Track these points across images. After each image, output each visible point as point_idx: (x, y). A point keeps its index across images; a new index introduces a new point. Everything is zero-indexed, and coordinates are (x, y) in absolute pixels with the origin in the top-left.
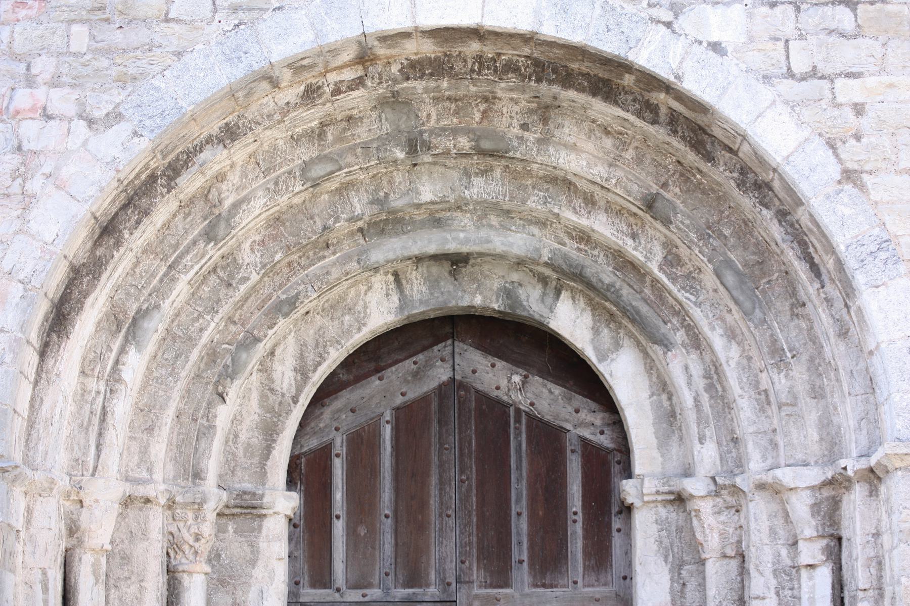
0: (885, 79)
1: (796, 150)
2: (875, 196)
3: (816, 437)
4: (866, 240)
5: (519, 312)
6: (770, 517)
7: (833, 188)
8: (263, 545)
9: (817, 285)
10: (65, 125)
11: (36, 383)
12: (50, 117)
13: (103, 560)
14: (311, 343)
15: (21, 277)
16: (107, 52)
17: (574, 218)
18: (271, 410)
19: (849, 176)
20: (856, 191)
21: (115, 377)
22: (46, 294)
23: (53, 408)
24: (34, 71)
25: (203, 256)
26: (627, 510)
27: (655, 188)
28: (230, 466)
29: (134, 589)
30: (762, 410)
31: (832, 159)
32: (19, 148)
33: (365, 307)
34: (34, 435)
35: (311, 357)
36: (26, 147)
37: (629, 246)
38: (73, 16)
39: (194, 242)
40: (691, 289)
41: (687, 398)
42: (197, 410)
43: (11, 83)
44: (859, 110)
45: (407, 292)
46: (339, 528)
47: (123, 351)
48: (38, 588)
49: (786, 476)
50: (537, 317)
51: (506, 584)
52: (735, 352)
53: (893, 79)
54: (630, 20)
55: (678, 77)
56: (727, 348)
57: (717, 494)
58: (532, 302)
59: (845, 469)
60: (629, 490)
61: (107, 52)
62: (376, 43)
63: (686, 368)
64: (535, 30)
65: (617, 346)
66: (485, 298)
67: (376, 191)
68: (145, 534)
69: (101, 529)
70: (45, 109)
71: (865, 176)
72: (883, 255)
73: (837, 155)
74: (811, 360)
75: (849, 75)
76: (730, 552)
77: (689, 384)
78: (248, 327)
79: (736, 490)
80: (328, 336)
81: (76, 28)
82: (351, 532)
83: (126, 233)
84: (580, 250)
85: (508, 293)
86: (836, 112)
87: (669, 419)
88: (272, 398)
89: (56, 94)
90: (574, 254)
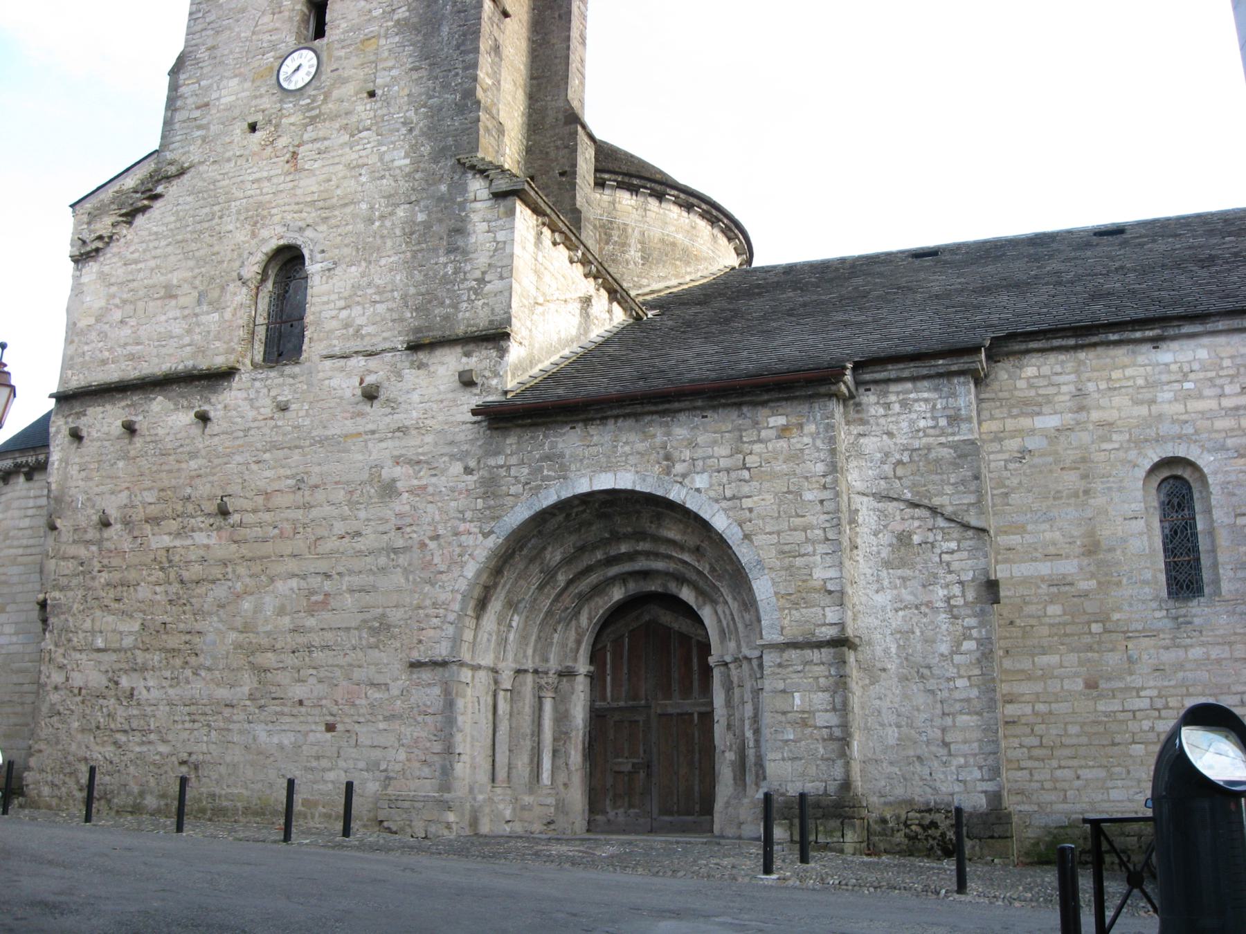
16: (489, 508)
21: (510, 626)
44: (751, 510)
46: (609, 678)
58: (673, 587)
61: (489, 508)
82: (613, 679)
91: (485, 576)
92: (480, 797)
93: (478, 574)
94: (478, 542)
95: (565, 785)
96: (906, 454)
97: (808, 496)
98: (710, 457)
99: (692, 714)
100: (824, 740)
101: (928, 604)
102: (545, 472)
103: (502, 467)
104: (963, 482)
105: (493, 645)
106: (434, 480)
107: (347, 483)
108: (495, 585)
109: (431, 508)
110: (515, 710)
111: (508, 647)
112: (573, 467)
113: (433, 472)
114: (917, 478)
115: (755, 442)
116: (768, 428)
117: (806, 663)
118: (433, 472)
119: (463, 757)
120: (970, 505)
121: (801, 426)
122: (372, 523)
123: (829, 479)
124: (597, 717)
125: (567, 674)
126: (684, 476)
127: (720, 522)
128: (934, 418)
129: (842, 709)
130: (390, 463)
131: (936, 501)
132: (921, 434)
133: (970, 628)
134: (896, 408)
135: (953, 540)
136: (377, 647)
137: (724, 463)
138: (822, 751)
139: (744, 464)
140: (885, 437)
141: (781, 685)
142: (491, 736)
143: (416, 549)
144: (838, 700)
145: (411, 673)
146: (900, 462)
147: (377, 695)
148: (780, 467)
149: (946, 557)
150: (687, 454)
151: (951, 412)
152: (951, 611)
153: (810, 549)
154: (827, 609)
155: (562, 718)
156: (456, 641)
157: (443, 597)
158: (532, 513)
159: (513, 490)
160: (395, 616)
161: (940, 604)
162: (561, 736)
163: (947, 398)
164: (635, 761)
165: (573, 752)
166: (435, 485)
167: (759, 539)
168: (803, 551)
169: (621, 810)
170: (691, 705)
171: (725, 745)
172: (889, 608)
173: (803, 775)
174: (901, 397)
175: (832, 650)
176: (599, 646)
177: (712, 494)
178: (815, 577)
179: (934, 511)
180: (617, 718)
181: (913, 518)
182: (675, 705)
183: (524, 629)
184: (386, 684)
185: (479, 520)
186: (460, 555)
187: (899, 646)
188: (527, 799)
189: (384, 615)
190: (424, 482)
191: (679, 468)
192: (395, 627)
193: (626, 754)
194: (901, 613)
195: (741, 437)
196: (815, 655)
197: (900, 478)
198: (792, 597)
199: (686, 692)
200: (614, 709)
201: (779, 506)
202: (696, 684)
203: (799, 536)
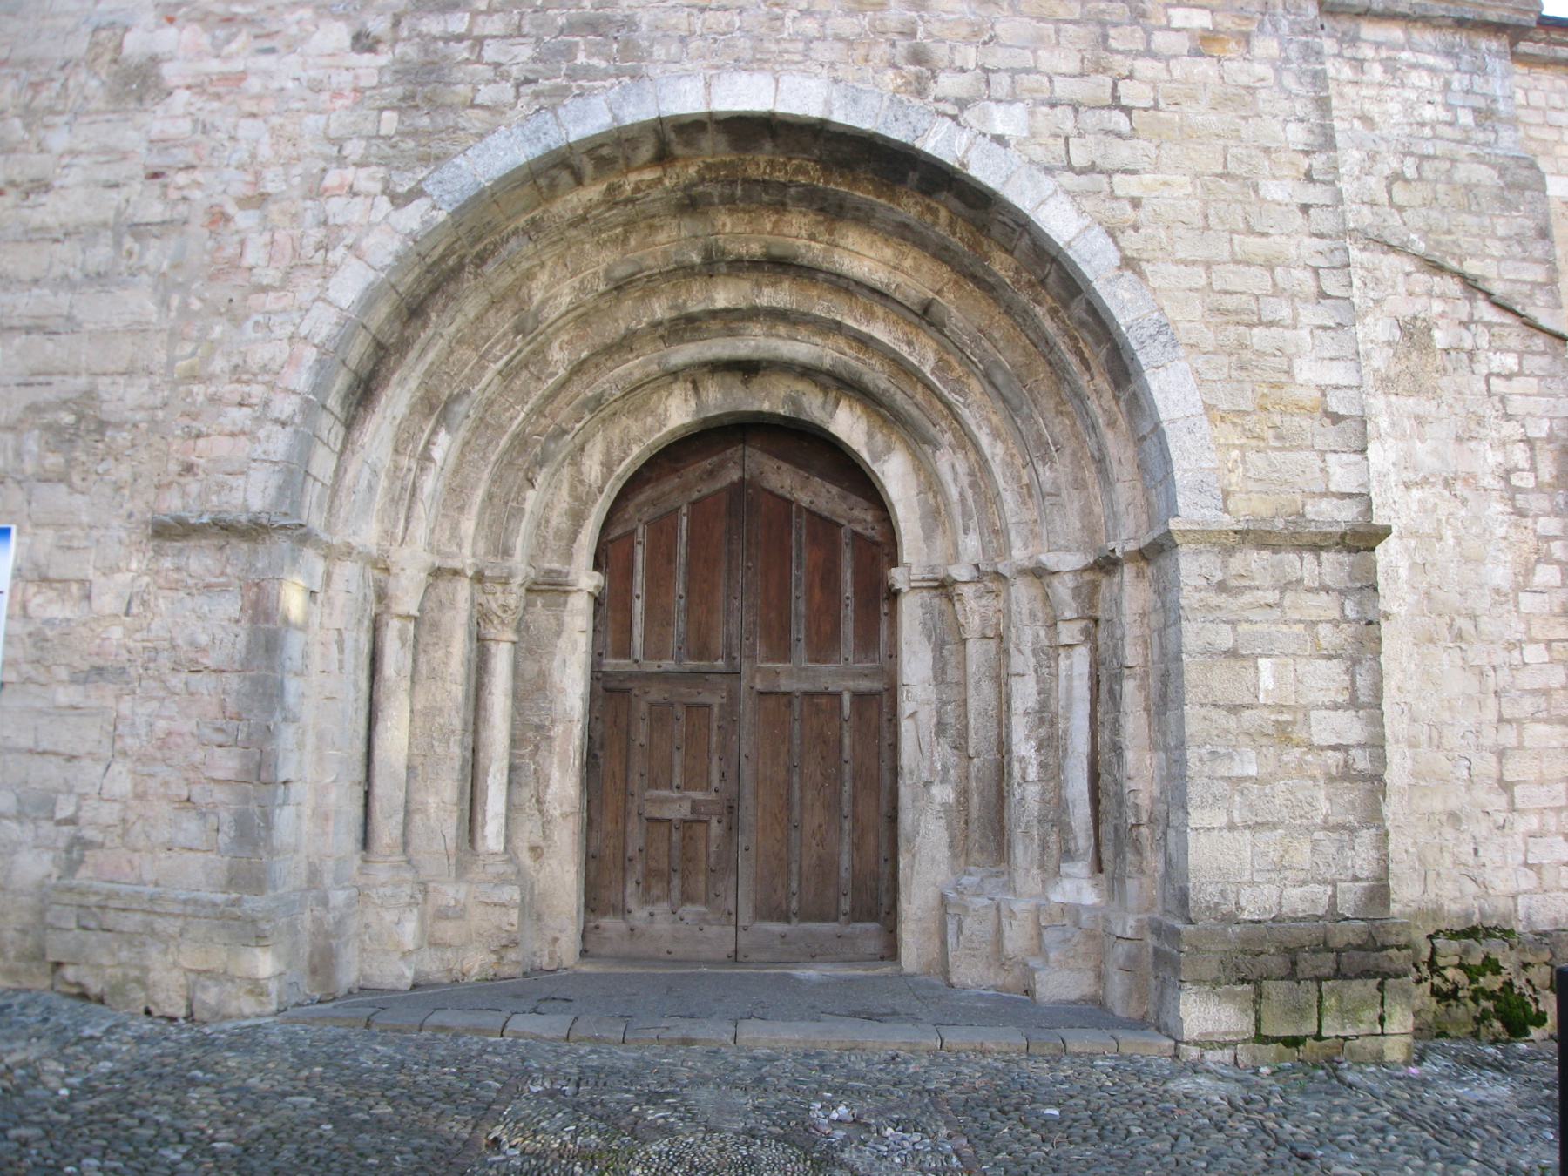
0: (1159, 177)
1: (1077, 236)
2: (1153, 282)
3: (1078, 525)
4: (1145, 323)
5: (803, 417)
6: (1032, 600)
7: (1112, 273)
8: (567, 619)
9: (1087, 377)
10: (369, 201)
11: (341, 454)
12: (355, 194)
13: (411, 626)
14: (617, 440)
15: (316, 341)
16: (414, 133)
17: (855, 325)
18: (577, 498)
19: (1129, 263)
20: (1134, 277)
21: (426, 457)
22: (344, 362)
23: (357, 478)
24: (345, 153)
25: (512, 347)
26: (894, 595)
27: (931, 295)
28: (540, 548)
29: (440, 654)
30: (1024, 503)
31: (1112, 246)
32: (325, 223)
33: (666, 410)
34: (337, 502)
35: (616, 453)
36: (331, 221)
37: (904, 350)
38: (384, 103)
39: (504, 335)
40: (959, 392)
41: (954, 493)
42: (508, 494)
43: (322, 164)
44: (1136, 203)
45: (703, 398)
46: (638, 606)
47: (434, 432)
48: (335, 648)
49: (1050, 560)
50: (818, 422)
51: (786, 657)
52: (999, 449)
53: (1167, 178)
54: (917, 112)
55: (962, 164)
56: (993, 446)
57: (979, 580)
58: (814, 406)
59: (1113, 551)
60: (898, 577)
61: (414, 133)
62: (673, 136)
63: (953, 466)
64: (825, 116)
65: (889, 449)
66: (772, 404)
67: (676, 298)
68: (453, 602)
69: (407, 598)
70: (351, 187)
71: (1144, 265)
72: (1162, 338)
73: (1116, 243)
74: (1074, 454)
75: (1125, 172)
76: (990, 633)
77: (955, 480)
78: (558, 420)
79: (998, 576)
80: (631, 435)
81: (386, 114)
82: (649, 608)
83: (434, 316)
84: (858, 359)
85: (794, 401)
86: (1115, 204)
87: (935, 517)
88: (580, 488)
89: (363, 173)
90: (854, 363)
91: (383, 310)
92: (338, 897)
93: (370, 299)
94: (377, 216)
95: (536, 851)
96: (1410, 162)
97: (1274, 191)
98: (1027, 71)
99: (839, 695)
100: (1331, 779)
101: (1470, 479)
102: (581, 59)
103: (459, 38)
104: (1519, 238)
105: (379, 499)
106: (266, 62)
107: (28, 63)
108: (404, 345)
109: (247, 129)
110: (424, 669)
111: (420, 510)
112: (659, 52)
113: (266, 44)
114: (1434, 214)
115: (1138, 54)
116: (1168, 28)
117: (1286, 586)
118: (266, 44)
119: (293, 788)
120: (1534, 284)
121: (1246, 39)
122: (83, 160)
123: (1318, 161)
124: (608, 692)
125: (551, 587)
126: (962, 104)
127: (1059, 221)
128: (1449, 107)
129: (1367, 702)
130: (149, 18)
131: (1472, 267)
132: (1427, 131)
133: (1548, 539)
134: (1376, 72)
135: (1508, 350)
136: (63, 478)
137: (1063, 88)
138: (1324, 806)
139: (1115, 97)
140: (1357, 123)
141: (1225, 639)
142: (363, 732)
143: (197, 227)
144: (1364, 681)
145: (158, 552)
146: (1398, 177)
147: (57, 611)
148: (1199, 115)
149: (1498, 385)
150: (969, 56)
151: (1481, 103)
152: (1512, 499)
153: (1285, 313)
154: (1331, 458)
155: (531, 691)
156: (294, 475)
157: (262, 354)
158: (537, 151)
159: (486, 94)
160: (125, 398)
161: (1490, 481)
162: (529, 735)
163: (1472, 74)
164: (699, 796)
165: (555, 774)
166: (268, 74)
167: (1162, 274)
168: (1267, 316)
169: (662, 908)
170: (842, 675)
171: (932, 770)
172: (1393, 478)
173: (1279, 867)
174: (1384, 54)
175: (1346, 558)
176: (617, 531)
177: (1038, 153)
178: (1300, 379)
179: (1471, 285)
180: (656, 694)
181: (1430, 294)
182: (797, 674)
183: (456, 472)
184: (82, 582)
185: (384, 161)
186: (323, 247)
187: (1413, 565)
188: (451, 893)
189: (90, 395)
190: (237, 65)
191: (948, 84)
192: (119, 426)
193: (677, 781)
194: (1416, 493)
195: (1105, 37)
196: (1306, 567)
197: (1401, 209)
198: (1249, 421)
199: (824, 645)
200: (649, 676)
201: (1206, 203)
202: (848, 629)
203: (1256, 280)
